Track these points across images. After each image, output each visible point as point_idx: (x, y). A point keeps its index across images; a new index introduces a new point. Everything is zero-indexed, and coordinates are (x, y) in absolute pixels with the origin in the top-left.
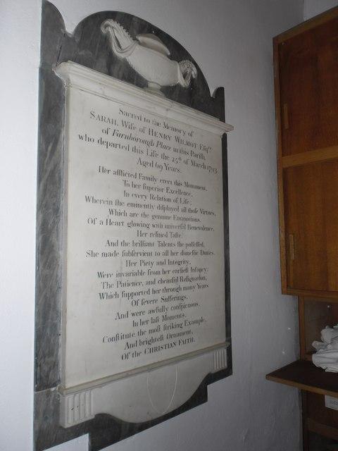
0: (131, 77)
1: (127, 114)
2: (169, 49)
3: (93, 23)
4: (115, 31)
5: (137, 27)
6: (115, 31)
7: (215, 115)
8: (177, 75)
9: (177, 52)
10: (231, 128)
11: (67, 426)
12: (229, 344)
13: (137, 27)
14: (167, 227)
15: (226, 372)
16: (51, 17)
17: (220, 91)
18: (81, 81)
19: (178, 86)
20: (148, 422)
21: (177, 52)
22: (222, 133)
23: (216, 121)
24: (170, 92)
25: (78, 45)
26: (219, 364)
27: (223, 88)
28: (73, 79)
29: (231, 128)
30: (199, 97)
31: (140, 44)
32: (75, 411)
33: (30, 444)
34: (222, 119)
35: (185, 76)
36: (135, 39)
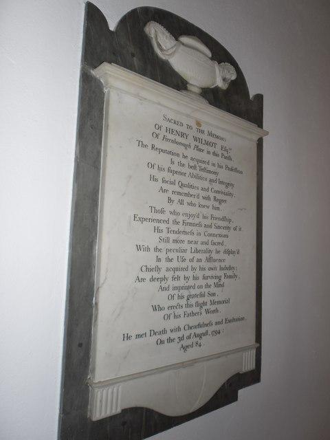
0: (176, 82)
1: (170, 121)
2: (157, 56)
3: (136, 20)
4: (155, 31)
5: (178, 27)
6: (155, 31)
7: (249, 119)
8: (220, 77)
9: (220, 55)
10: (267, 133)
11: (94, 419)
12: (258, 345)
13: (178, 27)
14: (190, 242)
15: (253, 377)
16: (94, 16)
17: (259, 98)
18: (119, 83)
19: (217, 89)
20: (223, 385)
21: (220, 55)
22: (256, 138)
23: (253, 127)
24: (213, 96)
25: (115, 44)
26: (249, 366)
27: (262, 96)
28: (112, 81)
29: (267, 133)
30: (235, 100)
31: (183, 44)
32: (105, 404)
33: (55, 436)
34: (260, 125)
35: (224, 80)
36: (177, 39)
